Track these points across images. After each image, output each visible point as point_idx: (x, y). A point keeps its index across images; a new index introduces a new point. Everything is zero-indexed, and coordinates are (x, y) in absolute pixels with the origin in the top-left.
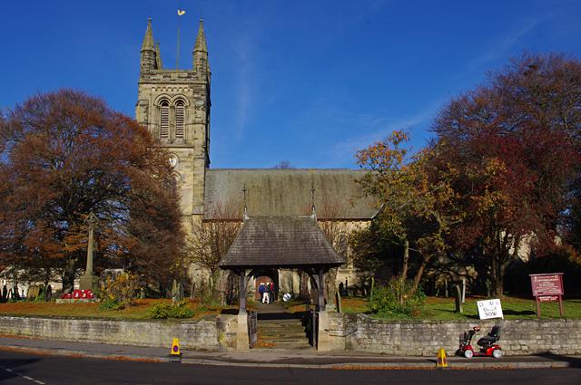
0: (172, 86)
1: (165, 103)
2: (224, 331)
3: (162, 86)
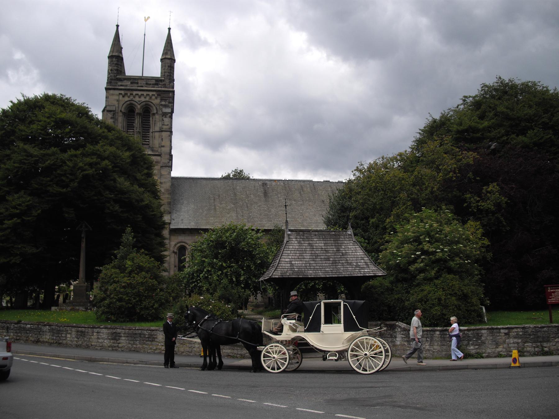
0: (140, 93)
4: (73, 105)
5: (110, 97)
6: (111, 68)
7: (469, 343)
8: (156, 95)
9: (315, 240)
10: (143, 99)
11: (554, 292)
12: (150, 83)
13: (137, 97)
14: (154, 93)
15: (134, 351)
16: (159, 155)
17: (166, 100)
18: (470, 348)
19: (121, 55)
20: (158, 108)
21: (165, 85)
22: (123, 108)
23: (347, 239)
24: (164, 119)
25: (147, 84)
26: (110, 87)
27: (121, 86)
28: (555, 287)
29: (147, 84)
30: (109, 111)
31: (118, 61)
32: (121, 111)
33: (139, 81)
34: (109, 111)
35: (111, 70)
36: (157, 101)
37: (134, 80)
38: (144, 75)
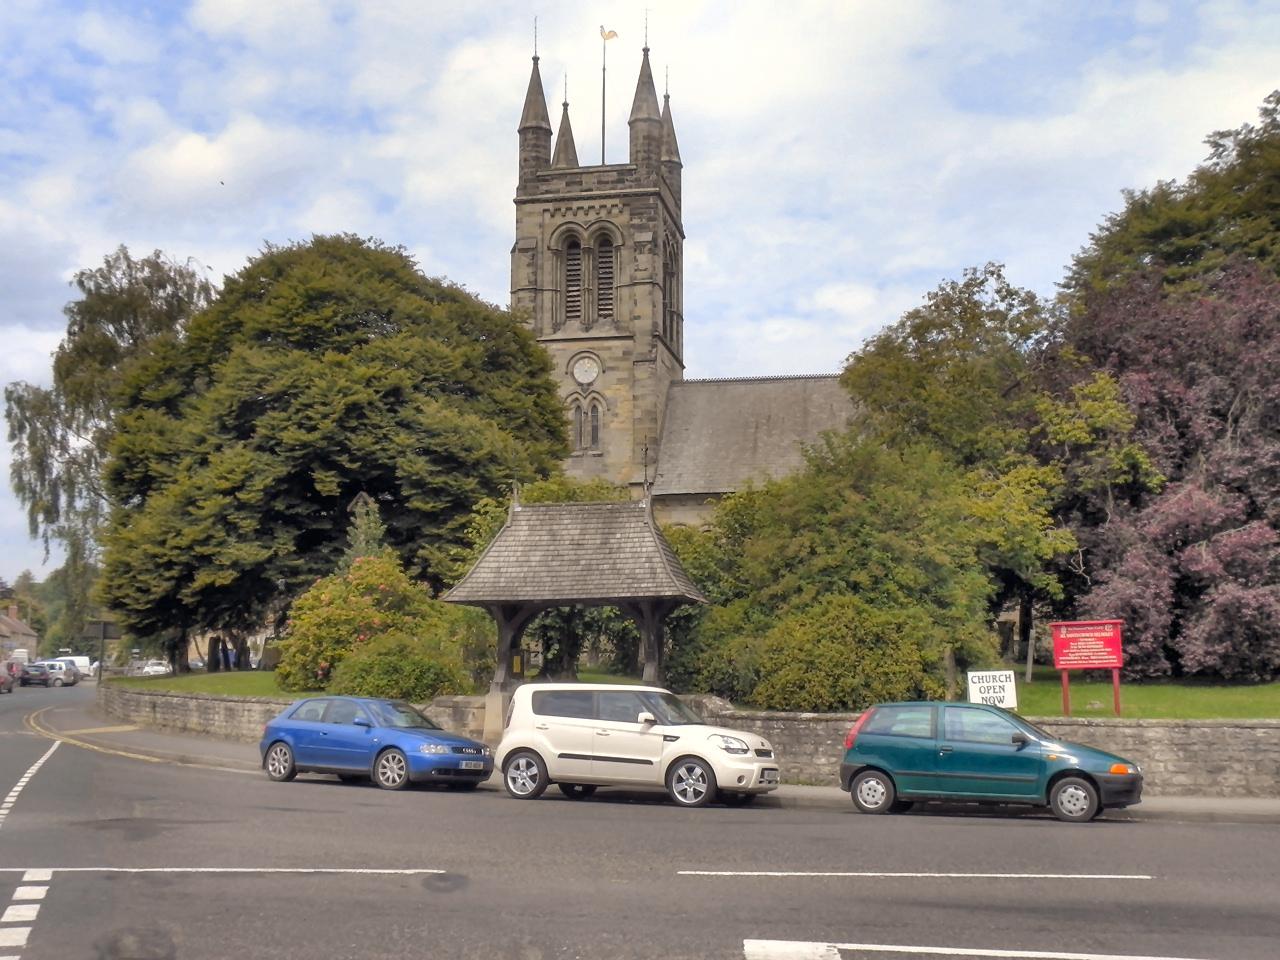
0: (586, 204)
1: (572, 242)
2: (464, 725)
3: (563, 206)
4: (309, 250)
5: (524, 220)
6: (524, 155)
7: (817, 750)
8: (620, 206)
9: (566, 522)
10: (592, 216)
11: (1075, 640)
12: (606, 179)
13: (581, 213)
14: (616, 201)
15: (227, 737)
16: (630, 338)
17: (642, 214)
18: (819, 762)
19: (544, 125)
20: (625, 233)
21: (637, 180)
22: (553, 240)
23: (634, 519)
24: (639, 257)
25: (599, 182)
26: (524, 198)
27: (547, 192)
28: (1092, 625)
29: (599, 182)
30: (524, 250)
31: (537, 139)
32: (549, 248)
33: (585, 178)
34: (524, 250)
35: (525, 160)
36: (624, 218)
37: (589, 171)
38: (607, 163)
